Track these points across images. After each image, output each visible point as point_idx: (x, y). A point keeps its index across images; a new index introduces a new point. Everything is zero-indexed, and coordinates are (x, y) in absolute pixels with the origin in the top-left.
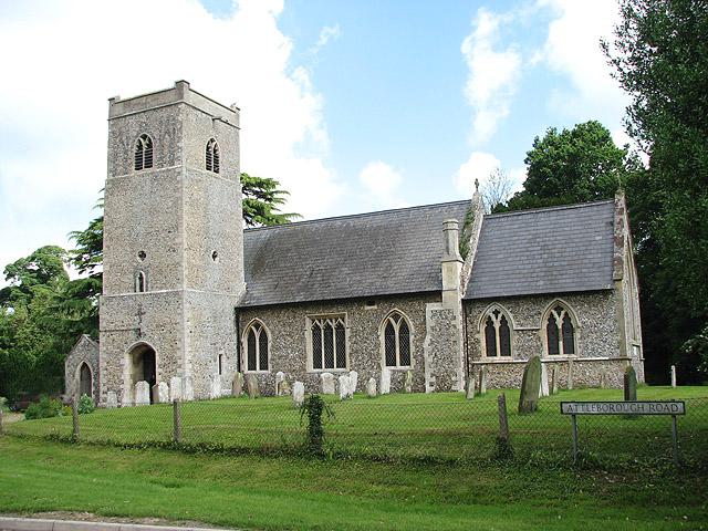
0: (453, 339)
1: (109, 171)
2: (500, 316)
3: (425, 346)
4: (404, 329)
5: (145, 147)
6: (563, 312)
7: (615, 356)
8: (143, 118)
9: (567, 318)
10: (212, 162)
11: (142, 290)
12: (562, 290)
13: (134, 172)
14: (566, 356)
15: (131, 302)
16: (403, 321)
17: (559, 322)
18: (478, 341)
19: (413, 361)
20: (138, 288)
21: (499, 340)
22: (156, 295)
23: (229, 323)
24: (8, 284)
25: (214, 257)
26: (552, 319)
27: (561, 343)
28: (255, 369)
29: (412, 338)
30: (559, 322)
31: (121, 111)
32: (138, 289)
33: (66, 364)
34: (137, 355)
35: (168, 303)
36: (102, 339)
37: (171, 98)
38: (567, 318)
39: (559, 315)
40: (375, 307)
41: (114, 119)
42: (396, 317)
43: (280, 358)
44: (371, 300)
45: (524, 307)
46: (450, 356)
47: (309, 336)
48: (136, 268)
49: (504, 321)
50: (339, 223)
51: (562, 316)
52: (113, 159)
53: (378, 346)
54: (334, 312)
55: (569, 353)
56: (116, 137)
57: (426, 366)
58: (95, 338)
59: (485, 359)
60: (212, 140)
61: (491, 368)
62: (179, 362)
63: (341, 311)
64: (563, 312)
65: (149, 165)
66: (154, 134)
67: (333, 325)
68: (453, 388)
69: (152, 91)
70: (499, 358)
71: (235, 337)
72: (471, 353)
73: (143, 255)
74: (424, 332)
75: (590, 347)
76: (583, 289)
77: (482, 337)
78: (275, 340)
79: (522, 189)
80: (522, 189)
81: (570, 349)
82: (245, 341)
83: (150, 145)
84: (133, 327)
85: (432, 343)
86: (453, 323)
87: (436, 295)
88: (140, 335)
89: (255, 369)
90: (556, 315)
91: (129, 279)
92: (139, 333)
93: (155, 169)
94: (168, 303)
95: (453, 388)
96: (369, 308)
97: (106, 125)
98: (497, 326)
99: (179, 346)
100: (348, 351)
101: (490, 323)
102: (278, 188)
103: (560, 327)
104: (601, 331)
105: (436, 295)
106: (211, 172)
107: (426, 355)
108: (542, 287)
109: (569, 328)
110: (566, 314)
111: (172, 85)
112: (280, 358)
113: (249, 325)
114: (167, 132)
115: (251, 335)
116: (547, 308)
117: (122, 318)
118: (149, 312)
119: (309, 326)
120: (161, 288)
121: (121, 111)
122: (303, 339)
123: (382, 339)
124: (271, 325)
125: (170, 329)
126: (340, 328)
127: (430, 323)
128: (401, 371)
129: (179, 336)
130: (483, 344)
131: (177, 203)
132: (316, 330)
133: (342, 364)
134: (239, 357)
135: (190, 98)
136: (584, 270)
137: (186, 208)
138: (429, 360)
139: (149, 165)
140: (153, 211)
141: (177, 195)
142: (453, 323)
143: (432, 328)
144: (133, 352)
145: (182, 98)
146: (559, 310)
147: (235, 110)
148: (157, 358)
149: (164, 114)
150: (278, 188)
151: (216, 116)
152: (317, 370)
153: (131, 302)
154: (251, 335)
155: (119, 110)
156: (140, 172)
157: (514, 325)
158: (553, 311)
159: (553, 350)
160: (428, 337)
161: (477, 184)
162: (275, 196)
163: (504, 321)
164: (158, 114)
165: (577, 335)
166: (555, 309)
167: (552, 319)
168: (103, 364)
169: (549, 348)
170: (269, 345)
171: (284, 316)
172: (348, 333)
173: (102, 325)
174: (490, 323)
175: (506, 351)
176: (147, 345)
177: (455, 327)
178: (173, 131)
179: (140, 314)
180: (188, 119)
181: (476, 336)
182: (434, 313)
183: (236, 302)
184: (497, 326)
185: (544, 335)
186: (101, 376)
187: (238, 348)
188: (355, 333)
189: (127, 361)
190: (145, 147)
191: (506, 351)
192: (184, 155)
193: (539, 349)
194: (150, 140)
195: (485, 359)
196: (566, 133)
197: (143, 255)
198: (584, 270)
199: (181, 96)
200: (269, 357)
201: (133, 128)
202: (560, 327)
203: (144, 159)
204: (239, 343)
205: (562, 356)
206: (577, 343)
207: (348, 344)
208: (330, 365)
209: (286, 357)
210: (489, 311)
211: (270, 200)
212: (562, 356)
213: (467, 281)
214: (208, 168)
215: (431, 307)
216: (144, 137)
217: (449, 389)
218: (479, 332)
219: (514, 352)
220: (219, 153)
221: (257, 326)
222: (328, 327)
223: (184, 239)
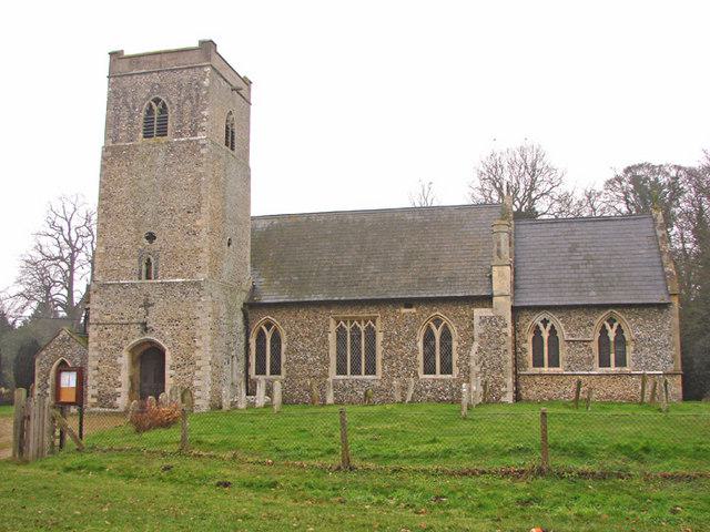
0: (503, 347)
1: (107, 136)
2: (549, 325)
3: (470, 354)
4: (446, 336)
6: (616, 325)
7: (669, 370)
8: (156, 78)
9: (620, 331)
11: (148, 278)
14: (618, 369)
16: (276, 329)
17: (612, 334)
20: (144, 273)
21: (548, 350)
22: (169, 284)
25: (229, 244)
26: (604, 331)
27: (612, 356)
29: (455, 345)
30: (612, 334)
33: (37, 360)
34: (137, 354)
35: (186, 294)
37: (195, 59)
38: (620, 331)
39: (612, 326)
40: (414, 310)
42: (437, 321)
43: (296, 362)
44: (409, 303)
45: (575, 317)
46: (500, 366)
47: (332, 338)
49: (553, 331)
51: (548, 327)
52: (112, 123)
53: (415, 352)
54: (364, 313)
55: (539, 366)
56: (117, 99)
59: (531, 370)
61: (538, 379)
62: (198, 363)
64: (616, 325)
66: (171, 99)
67: (362, 328)
68: (503, 399)
70: (545, 370)
71: (243, 336)
72: (518, 364)
73: (151, 237)
76: (640, 302)
77: (529, 347)
78: (290, 341)
81: (621, 362)
82: (253, 341)
83: (164, 110)
84: (135, 320)
85: (480, 350)
86: (504, 330)
87: (487, 300)
88: (146, 329)
90: (434, 327)
91: (132, 264)
92: (145, 328)
94: (186, 294)
95: (503, 399)
96: (404, 311)
98: (545, 335)
99: (198, 344)
100: (379, 357)
101: (537, 332)
103: (612, 339)
104: (655, 344)
108: (594, 298)
110: (619, 326)
111: (196, 45)
112: (296, 362)
113: (259, 322)
115: (261, 335)
116: (600, 319)
117: (121, 310)
118: (160, 304)
119: (333, 327)
120: (176, 276)
122: (325, 342)
124: (285, 325)
126: (371, 334)
127: (478, 330)
128: (442, 380)
129: (198, 333)
130: (530, 353)
132: (341, 334)
136: (635, 283)
139: (163, 132)
140: (167, 187)
142: (504, 330)
143: (480, 336)
144: (132, 350)
145: (209, 60)
149: (185, 77)
152: (342, 377)
155: (123, 67)
156: (151, 141)
157: (563, 334)
159: (604, 362)
160: (476, 345)
163: (553, 331)
164: (176, 76)
165: (630, 349)
167: (604, 331)
170: (284, 347)
171: (303, 315)
172: (380, 337)
174: (537, 332)
175: (554, 362)
176: (151, 342)
178: (195, 96)
179: (147, 305)
181: (524, 345)
184: (545, 335)
185: (595, 346)
188: (388, 338)
189: (124, 359)
193: (590, 361)
194: (164, 105)
195: (531, 370)
197: (151, 237)
198: (635, 283)
199: (208, 58)
202: (612, 339)
203: (156, 124)
206: (629, 357)
208: (356, 371)
210: (537, 319)
215: (479, 312)
217: (498, 399)
221: (268, 325)
222: (355, 329)
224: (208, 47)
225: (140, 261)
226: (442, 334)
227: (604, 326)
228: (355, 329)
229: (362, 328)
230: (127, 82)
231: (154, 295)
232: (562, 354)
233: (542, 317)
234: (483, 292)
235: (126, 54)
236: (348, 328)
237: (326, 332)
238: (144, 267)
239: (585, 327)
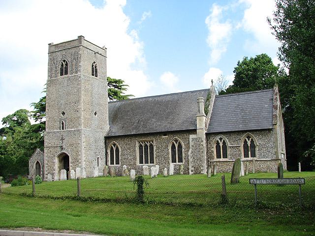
0: (201, 151)
1: (49, 76)
2: (222, 140)
4: (180, 146)
5: (64, 65)
6: (250, 139)
7: (274, 158)
9: (252, 141)
10: (95, 72)
11: (63, 129)
12: (250, 129)
13: (59, 77)
14: (252, 158)
15: (58, 134)
16: (179, 143)
17: (249, 143)
18: (213, 152)
19: (184, 160)
20: (61, 128)
21: (222, 151)
23: (102, 144)
24: (4, 126)
25: (95, 114)
26: (245, 142)
27: (250, 152)
28: (113, 164)
29: (183, 150)
30: (249, 143)
31: (54, 49)
32: (61, 129)
33: (29, 162)
36: (45, 151)
37: (76, 44)
38: (252, 141)
39: (249, 140)
40: (167, 136)
41: (51, 53)
42: (176, 141)
43: (125, 159)
44: (165, 133)
45: (233, 136)
46: (200, 158)
48: (60, 119)
49: (224, 143)
50: (151, 99)
51: (250, 140)
52: (50, 70)
53: (168, 154)
54: (149, 139)
55: (253, 157)
56: (52, 61)
57: (190, 163)
58: (42, 150)
59: (216, 159)
60: (94, 62)
61: (218, 163)
63: (152, 138)
64: (250, 139)
65: (66, 73)
66: (69, 59)
67: (148, 145)
68: (202, 172)
69: (68, 41)
70: (222, 159)
71: (104, 150)
72: (209, 157)
73: (63, 113)
74: (189, 148)
75: (263, 154)
76: (260, 128)
78: (122, 151)
79: (232, 84)
80: (232, 84)
81: (253, 155)
83: (67, 65)
84: (59, 145)
85: (192, 152)
86: (202, 143)
87: (194, 131)
88: (62, 149)
89: (113, 164)
90: (247, 140)
91: (57, 124)
92: (62, 148)
93: (69, 75)
95: (202, 172)
96: (164, 137)
97: (47, 55)
98: (221, 145)
99: (80, 154)
100: (155, 156)
101: (218, 143)
102: (124, 83)
103: (249, 145)
104: (267, 147)
105: (194, 131)
106: (94, 77)
107: (189, 158)
108: (241, 127)
109: (253, 146)
110: (252, 140)
111: (76, 38)
112: (125, 159)
113: (111, 144)
114: (74, 59)
115: (112, 149)
116: (243, 137)
117: (54, 142)
118: (67, 139)
119: (137, 145)
120: (72, 128)
121: (54, 49)
122: (135, 151)
123: (170, 151)
124: (120, 145)
125: (76, 146)
126: (151, 146)
127: (191, 143)
128: (178, 165)
129: (79, 149)
130: (215, 153)
131: (79, 91)
132: (141, 146)
133: (152, 162)
134: (106, 158)
135: (84, 43)
136: (260, 120)
137: (83, 92)
138: (191, 160)
139: (66, 73)
140: (68, 94)
141: (79, 87)
142: (202, 143)
143: (192, 146)
144: (59, 156)
145: (81, 43)
146: (249, 138)
147: (104, 49)
148: (70, 159)
149: (73, 51)
150: (124, 83)
151: (96, 51)
153: (58, 134)
154: (112, 149)
155: (53, 49)
157: (229, 144)
158: (246, 138)
159: (246, 155)
160: (191, 150)
161: (212, 82)
162: (123, 87)
163: (224, 143)
164: (70, 51)
165: (257, 149)
166: (247, 137)
167: (245, 142)
168: (46, 162)
169: (244, 155)
170: (120, 153)
171: (126, 140)
172: (155, 148)
173: (46, 144)
174: (218, 143)
175: (225, 156)
176: (65, 154)
177: (202, 145)
178: (77, 58)
179: (62, 139)
180: (83, 53)
181: (212, 149)
182: (193, 139)
183: (105, 134)
184: (221, 145)
185: (242, 149)
186: (45, 167)
187: (106, 155)
188: (158, 148)
189: (56, 160)
190: (64, 65)
191: (225, 156)
192: (82, 69)
193: (240, 155)
194: (67, 62)
195: (216, 159)
196: (252, 59)
197: (63, 113)
198: (260, 120)
199: (81, 43)
200: (120, 159)
201: (59, 57)
202: (249, 145)
203: (64, 71)
204: (106, 153)
205: (250, 158)
206: (257, 152)
207: (155, 153)
208: (147, 162)
209: (127, 159)
210: (218, 138)
211: (120, 89)
212: (250, 158)
213: (208, 125)
214: (93, 75)
215: (192, 136)
216: (64, 61)
217: (200, 173)
218: (213, 148)
219: (229, 157)
220: (98, 68)
221: (114, 145)
222: (146, 146)
223: (82, 106)
224: (80, 37)
225: (60, 123)
226: (178, 146)
227: (245, 140)
228: (146, 146)
229: (148, 145)
230: (54, 54)
231: (65, 134)
232: (228, 153)
233: (219, 137)
234: (269, 126)
235: (54, 44)
236: (143, 145)
237: (135, 147)
238: (61, 125)
239: (237, 141)
